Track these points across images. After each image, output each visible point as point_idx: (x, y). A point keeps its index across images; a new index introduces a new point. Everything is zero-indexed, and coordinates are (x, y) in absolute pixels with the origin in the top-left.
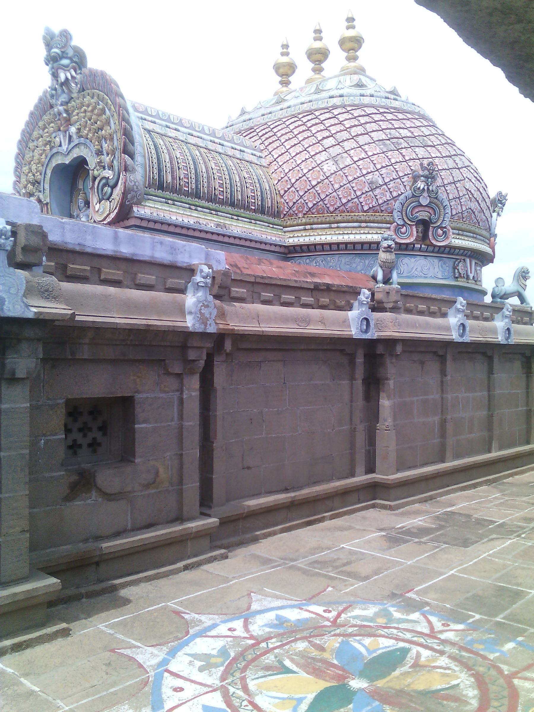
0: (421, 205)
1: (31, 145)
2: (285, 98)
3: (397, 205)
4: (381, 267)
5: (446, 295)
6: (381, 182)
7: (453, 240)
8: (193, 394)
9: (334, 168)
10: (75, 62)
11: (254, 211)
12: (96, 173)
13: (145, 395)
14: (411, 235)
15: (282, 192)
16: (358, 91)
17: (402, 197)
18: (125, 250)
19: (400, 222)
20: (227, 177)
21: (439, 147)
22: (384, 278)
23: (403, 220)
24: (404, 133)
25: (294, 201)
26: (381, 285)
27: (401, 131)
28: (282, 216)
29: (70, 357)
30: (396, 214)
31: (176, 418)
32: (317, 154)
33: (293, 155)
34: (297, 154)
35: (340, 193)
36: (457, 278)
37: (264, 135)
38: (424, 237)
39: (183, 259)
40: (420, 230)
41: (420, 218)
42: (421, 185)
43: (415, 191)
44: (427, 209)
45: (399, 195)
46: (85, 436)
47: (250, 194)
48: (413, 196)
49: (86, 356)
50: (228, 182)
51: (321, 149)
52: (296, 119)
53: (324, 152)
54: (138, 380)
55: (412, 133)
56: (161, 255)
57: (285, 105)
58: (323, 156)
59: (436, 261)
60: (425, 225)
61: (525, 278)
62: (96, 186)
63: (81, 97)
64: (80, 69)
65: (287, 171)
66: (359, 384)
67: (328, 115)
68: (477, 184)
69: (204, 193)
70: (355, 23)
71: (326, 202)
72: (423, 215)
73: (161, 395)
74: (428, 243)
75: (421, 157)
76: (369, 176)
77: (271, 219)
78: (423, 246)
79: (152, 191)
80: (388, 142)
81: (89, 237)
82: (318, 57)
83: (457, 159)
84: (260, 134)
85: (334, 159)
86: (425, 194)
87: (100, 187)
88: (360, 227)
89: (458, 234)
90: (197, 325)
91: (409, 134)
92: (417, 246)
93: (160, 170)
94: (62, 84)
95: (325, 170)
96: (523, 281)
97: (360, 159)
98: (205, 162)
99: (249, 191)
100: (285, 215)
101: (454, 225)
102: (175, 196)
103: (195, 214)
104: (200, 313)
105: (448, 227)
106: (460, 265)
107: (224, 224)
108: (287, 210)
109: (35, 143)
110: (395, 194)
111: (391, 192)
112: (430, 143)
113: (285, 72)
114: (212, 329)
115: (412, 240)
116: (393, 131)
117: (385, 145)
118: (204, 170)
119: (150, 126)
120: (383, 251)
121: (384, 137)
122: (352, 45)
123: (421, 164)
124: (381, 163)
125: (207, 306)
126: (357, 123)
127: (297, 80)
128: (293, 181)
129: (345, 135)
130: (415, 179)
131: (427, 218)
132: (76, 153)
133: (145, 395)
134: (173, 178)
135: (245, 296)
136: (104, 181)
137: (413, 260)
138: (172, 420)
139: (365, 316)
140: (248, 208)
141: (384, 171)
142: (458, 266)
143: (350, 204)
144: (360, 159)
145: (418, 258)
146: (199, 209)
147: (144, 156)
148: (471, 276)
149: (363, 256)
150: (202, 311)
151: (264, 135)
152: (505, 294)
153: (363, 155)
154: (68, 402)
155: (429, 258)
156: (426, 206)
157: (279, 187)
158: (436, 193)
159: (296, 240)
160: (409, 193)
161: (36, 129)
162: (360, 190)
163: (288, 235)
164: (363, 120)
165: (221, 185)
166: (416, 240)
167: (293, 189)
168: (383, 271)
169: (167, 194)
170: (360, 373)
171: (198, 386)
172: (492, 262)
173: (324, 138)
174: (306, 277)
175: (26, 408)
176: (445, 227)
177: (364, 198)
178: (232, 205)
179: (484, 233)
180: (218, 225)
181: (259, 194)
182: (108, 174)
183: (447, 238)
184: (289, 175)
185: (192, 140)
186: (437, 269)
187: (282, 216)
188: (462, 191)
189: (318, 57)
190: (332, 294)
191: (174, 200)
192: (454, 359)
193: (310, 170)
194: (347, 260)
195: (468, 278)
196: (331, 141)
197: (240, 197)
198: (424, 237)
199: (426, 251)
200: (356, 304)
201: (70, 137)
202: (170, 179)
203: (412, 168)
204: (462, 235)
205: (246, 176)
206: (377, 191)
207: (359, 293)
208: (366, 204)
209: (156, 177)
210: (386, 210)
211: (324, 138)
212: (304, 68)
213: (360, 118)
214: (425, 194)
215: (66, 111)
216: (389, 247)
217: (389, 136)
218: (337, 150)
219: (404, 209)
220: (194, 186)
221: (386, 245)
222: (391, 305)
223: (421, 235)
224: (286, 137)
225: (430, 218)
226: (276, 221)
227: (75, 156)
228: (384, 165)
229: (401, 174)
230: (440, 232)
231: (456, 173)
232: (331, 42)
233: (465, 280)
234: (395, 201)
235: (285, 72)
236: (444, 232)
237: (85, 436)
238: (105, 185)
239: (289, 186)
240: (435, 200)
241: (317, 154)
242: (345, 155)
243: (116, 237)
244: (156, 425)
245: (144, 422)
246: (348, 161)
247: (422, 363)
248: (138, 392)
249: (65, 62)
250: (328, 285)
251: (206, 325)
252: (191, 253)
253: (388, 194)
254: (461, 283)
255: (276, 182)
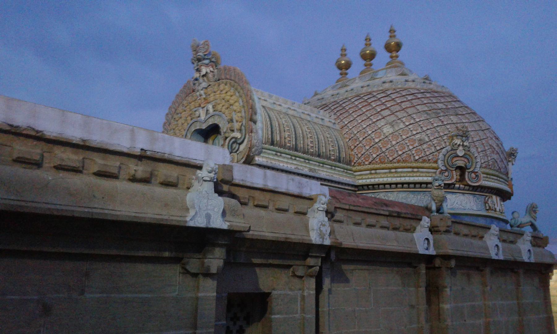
0: (458, 156)
1: (176, 116)
2: (347, 83)
3: (441, 156)
4: (434, 200)
5: (481, 222)
6: (427, 139)
7: (484, 182)
8: (312, 292)
9: (391, 130)
10: (213, 62)
11: (334, 160)
12: (227, 135)
13: (279, 292)
14: (453, 177)
15: (353, 147)
16: (404, 78)
17: (444, 150)
18: (271, 185)
19: (443, 168)
20: (316, 137)
21: (467, 116)
22: (437, 208)
23: (445, 166)
24: (440, 106)
25: (362, 153)
26: (435, 214)
27: (438, 105)
28: (353, 164)
29: (233, 261)
30: (440, 162)
31: (299, 312)
32: (378, 120)
33: (360, 121)
34: (363, 121)
35: (397, 147)
36: (487, 210)
37: (335, 108)
38: (462, 179)
39: (306, 192)
40: (458, 174)
41: (458, 165)
42: (458, 141)
43: (453, 146)
44: (462, 159)
45: (441, 149)
46: (235, 324)
47: (331, 149)
48: (452, 150)
49: (242, 261)
50: (316, 140)
51: (380, 117)
52: (359, 98)
53: (383, 120)
54: (275, 280)
55: (447, 106)
56: (293, 189)
57: (349, 88)
58: (382, 123)
59: (471, 197)
60: (462, 170)
61: (535, 212)
62: (227, 144)
63: (217, 85)
64: (216, 66)
65: (355, 132)
66: (422, 290)
67: (383, 95)
68: (497, 142)
69: (301, 148)
70: (396, 33)
71: (386, 154)
72: (461, 163)
73: (290, 293)
74: (465, 183)
75: (455, 122)
76: (418, 136)
77: (345, 166)
78: (461, 186)
79: (267, 146)
80: (429, 112)
81: (249, 175)
82: (368, 57)
83: (481, 123)
84: (332, 108)
85: (392, 124)
86: (461, 148)
87: (230, 144)
88: (413, 171)
89: (487, 177)
90: (318, 239)
91: (444, 107)
92: (457, 186)
93: (272, 133)
94: (203, 76)
95: (385, 132)
96: (534, 214)
97: (410, 124)
98: (301, 127)
99: (331, 146)
100: (355, 163)
101: (483, 170)
102: (282, 150)
103: (295, 162)
104: (320, 230)
105: (479, 172)
106: (490, 200)
107: (315, 169)
108: (356, 159)
109: (179, 115)
110: (438, 148)
111: (435, 147)
112: (460, 113)
113: (344, 67)
114: (327, 242)
115: (453, 181)
116: (432, 105)
117: (427, 114)
118: (301, 132)
119: (265, 103)
120: (435, 189)
121: (426, 109)
122: (393, 48)
123: (457, 127)
124: (426, 126)
125: (324, 225)
126: (405, 100)
127: (352, 72)
128: (361, 139)
129: (397, 108)
130: (452, 138)
131: (463, 165)
132: (211, 122)
133: (279, 292)
134: (280, 138)
135: (342, 219)
136: (233, 140)
137: (454, 196)
138: (297, 313)
139: (427, 237)
140: (329, 158)
141: (428, 132)
142: (488, 200)
143: (405, 155)
144: (410, 124)
145: (458, 195)
146: (297, 159)
147: (263, 123)
148: (498, 210)
149: (417, 193)
150: (321, 229)
151: (335, 108)
152: (521, 224)
153: (412, 121)
154: (229, 294)
155: (466, 195)
156: (461, 157)
157: (350, 143)
158: (469, 148)
159: (364, 181)
160: (449, 148)
161: (181, 106)
162: (412, 145)
163: (358, 177)
164: (409, 98)
165: (312, 142)
166: (456, 181)
167: (361, 145)
168: (436, 203)
169: (277, 148)
170: (423, 281)
171: (314, 287)
172: (510, 199)
173: (382, 110)
174: (382, 206)
175: (213, 296)
176: (477, 172)
177: (416, 150)
178: (319, 156)
179: (504, 177)
180: (311, 170)
181: (337, 148)
182: (237, 135)
183: (480, 180)
184: (358, 135)
185: (291, 112)
186: (472, 204)
187: (353, 164)
188: (487, 146)
189: (368, 57)
190: (401, 219)
191: (281, 153)
192: (492, 273)
193: (373, 132)
194: (403, 195)
195: (495, 211)
196: (387, 112)
197: (324, 151)
198: (462, 179)
199: (464, 190)
200: (418, 228)
201: (207, 110)
202: (278, 139)
203: (450, 130)
204: (490, 178)
205: (328, 136)
206: (425, 146)
207: (421, 220)
208: (417, 155)
209: (270, 137)
210: (432, 159)
211: (382, 110)
212: (358, 65)
213: (407, 96)
214: (461, 148)
215: (205, 93)
216: (440, 185)
217: (430, 108)
218: (392, 118)
219: (446, 158)
220: (294, 143)
221: (437, 184)
222: (444, 229)
223: (458, 177)
224: (353, 110)
225: (466, 166)
226: (349, 167)
227: (211, 123)
228: (428, 127)
229: (442, 134)
230: (473, 175)
231: (481, 133)
232: (378, 46)
233: (493, 212)
234: (439, 153)
235: (344, 67)
236: (476, 176)
237: (235, 324)
238: (234, 143)
239: (358, 143)
240: (468, 153)
241: (378, 120)
242: (399, 121)
243: (265, 176)
244: (286, 316)
245: (278, 314)
246: (402, 126)
247: (469, 276)
248: (274, 289)
249: (207, 62)
250: (398, 213)
251: (323, 239)
252: (312, 188)
253: (433, 148)
254: (491, 214)
255: (348, 140)
